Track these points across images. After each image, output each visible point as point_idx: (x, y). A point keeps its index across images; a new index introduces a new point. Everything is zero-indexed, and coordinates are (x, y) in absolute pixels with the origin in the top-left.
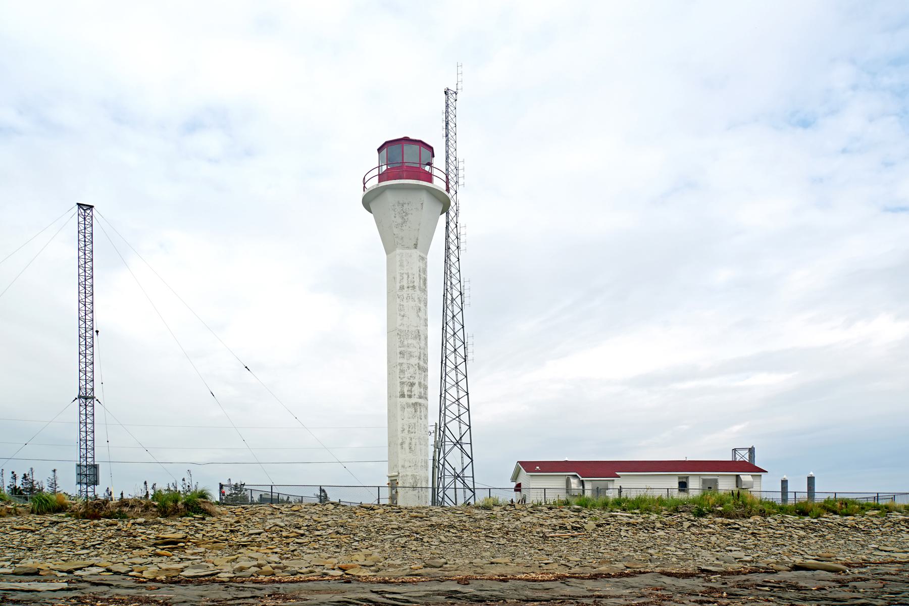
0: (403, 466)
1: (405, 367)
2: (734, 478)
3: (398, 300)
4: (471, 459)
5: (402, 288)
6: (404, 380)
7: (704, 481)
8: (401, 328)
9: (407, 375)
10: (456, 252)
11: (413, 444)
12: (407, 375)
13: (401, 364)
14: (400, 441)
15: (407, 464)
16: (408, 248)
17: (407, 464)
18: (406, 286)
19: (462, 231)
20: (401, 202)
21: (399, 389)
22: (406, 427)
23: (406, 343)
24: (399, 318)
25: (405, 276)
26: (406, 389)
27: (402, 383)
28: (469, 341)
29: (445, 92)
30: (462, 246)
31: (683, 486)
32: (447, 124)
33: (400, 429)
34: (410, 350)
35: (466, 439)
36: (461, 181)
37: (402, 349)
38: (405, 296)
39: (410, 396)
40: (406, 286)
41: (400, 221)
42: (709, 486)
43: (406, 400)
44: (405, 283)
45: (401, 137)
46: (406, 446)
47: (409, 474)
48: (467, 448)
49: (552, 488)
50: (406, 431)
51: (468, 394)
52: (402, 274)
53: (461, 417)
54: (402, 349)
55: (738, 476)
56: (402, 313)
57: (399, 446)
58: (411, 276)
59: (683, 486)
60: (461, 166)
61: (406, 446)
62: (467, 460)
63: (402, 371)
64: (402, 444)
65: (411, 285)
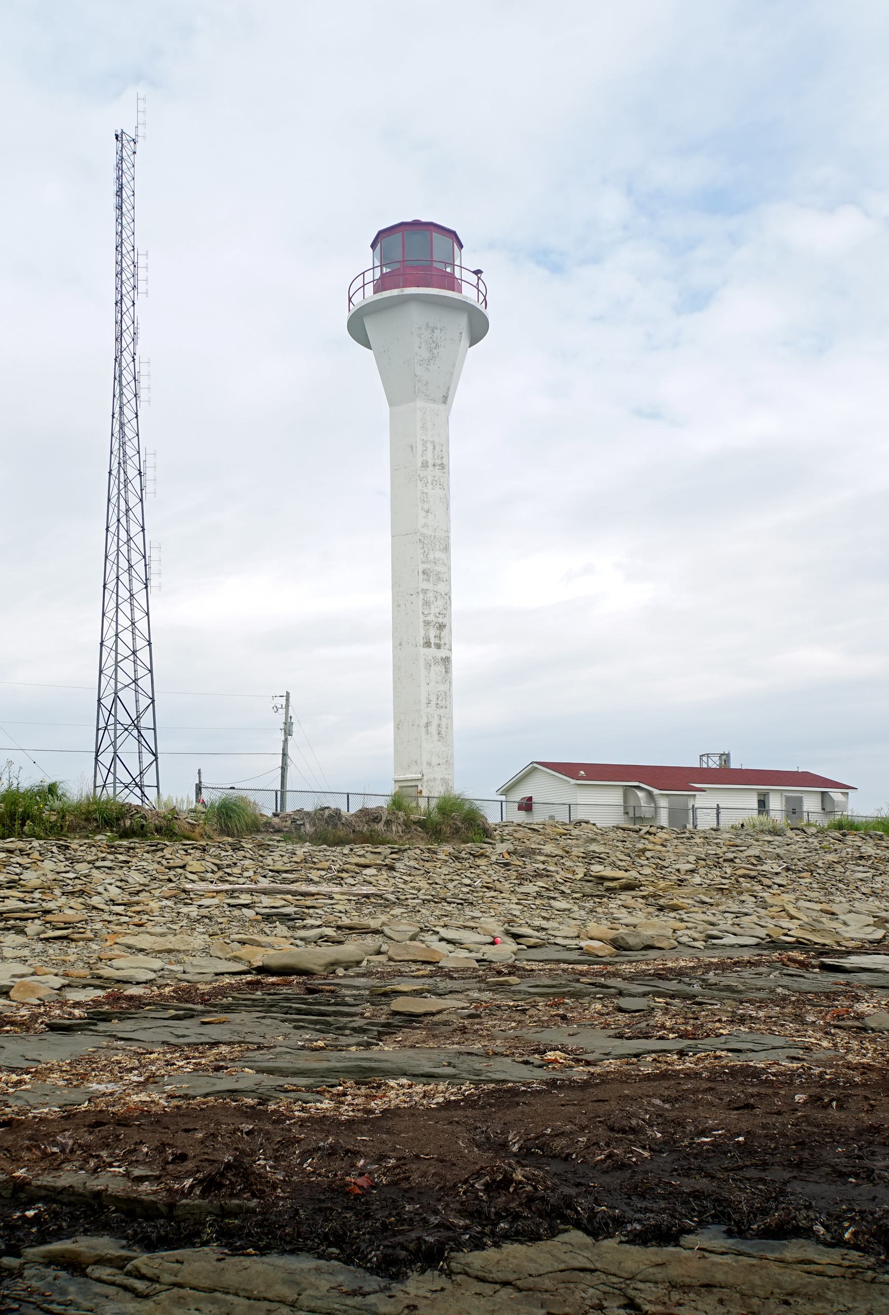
0: (429, 764)
1: (430, 595)
2: (819, 797)
3: (420, 484)
4: (155, 755)
5: (425, 465)
6: (431, 618)
7: (788, 799)
8: (424, 530)
9: (434, 610)
10: (133, 402)
11: (444, 726)
12: (434, 610)
13: (425, 591)
14: (424, 721)
15: (435, 761)
16: (434, 401)
17: (435, 761)
18: (431, 462)
19: (143, 369)
20: (431, 325)
21: (422, 633)
22: (433, 698)
23: (431, 556)
24: (422, 514)
25: (430, 447)
26: (432, 633)
27: (427, 623)
28: (151, 553)
29: (117, 137)
30: (143, 394)
31: (763, 805)
32: (121, 189)
33: (424, 701)
34: (438, 568)
35: (146, 721)
36: (141, 286)
37: (426, 566)
38: (430, 479)
39: (438, 646)
40: (431, 462)
41: (426, 354)
42: (794, 809)
43: (433, 651)
44: (429, 457)
45: (410, 220)
46: (433, 729)
47: (438, 776)
48: (148, 735)
49: (602, 806)
50: (433, 703)
51: (150, 644)
52: (424, 442)
53: (139, 682)
54: (426, 566)
55: (823, 793)
56: (426, 506)
57: (423, 730)
58: (438, 448)
59: (763, 805)
60: (142, 262)
61: (433, 729)
62: (148, 758)
63: (427, 603)
64: (427, 725)
65: (439, 462)
